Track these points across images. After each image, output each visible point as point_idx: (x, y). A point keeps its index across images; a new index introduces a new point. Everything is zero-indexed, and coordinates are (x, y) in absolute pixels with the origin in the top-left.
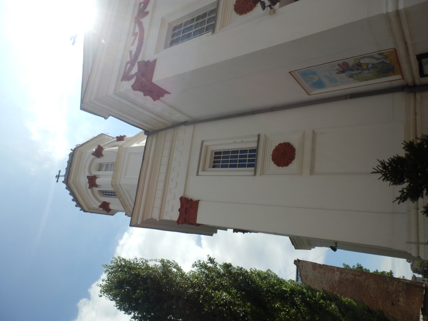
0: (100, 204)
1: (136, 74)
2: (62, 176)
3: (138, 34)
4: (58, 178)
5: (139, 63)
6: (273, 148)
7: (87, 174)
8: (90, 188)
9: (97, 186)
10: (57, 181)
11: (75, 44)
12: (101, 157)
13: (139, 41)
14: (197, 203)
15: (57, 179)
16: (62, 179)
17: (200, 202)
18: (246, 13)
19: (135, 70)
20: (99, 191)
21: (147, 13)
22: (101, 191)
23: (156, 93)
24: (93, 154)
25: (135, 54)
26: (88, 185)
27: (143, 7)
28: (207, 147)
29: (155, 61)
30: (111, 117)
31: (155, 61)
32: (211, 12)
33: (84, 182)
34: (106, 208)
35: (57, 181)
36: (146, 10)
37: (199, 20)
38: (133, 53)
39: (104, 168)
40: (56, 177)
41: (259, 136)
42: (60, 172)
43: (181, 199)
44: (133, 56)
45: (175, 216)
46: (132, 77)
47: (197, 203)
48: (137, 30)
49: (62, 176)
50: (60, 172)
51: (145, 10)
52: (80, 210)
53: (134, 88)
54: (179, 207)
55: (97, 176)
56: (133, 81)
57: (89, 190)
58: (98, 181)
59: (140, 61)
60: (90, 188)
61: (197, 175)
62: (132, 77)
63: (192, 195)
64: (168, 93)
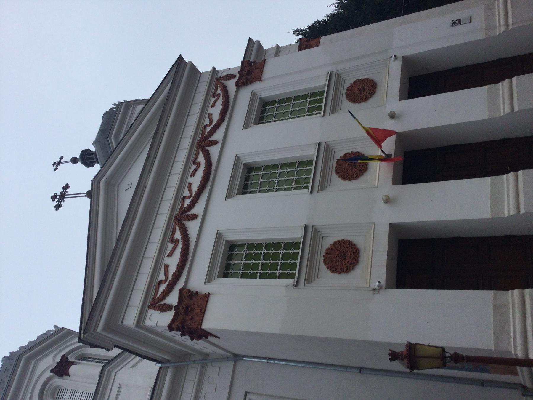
12: (65, 377)
18: (360, 102)
19: (173, 299)
31: (207, 297)
36: (193, 212)
46: (168, 308)
53: (171, 327)
56: (169, 316)
62: (168, 308)
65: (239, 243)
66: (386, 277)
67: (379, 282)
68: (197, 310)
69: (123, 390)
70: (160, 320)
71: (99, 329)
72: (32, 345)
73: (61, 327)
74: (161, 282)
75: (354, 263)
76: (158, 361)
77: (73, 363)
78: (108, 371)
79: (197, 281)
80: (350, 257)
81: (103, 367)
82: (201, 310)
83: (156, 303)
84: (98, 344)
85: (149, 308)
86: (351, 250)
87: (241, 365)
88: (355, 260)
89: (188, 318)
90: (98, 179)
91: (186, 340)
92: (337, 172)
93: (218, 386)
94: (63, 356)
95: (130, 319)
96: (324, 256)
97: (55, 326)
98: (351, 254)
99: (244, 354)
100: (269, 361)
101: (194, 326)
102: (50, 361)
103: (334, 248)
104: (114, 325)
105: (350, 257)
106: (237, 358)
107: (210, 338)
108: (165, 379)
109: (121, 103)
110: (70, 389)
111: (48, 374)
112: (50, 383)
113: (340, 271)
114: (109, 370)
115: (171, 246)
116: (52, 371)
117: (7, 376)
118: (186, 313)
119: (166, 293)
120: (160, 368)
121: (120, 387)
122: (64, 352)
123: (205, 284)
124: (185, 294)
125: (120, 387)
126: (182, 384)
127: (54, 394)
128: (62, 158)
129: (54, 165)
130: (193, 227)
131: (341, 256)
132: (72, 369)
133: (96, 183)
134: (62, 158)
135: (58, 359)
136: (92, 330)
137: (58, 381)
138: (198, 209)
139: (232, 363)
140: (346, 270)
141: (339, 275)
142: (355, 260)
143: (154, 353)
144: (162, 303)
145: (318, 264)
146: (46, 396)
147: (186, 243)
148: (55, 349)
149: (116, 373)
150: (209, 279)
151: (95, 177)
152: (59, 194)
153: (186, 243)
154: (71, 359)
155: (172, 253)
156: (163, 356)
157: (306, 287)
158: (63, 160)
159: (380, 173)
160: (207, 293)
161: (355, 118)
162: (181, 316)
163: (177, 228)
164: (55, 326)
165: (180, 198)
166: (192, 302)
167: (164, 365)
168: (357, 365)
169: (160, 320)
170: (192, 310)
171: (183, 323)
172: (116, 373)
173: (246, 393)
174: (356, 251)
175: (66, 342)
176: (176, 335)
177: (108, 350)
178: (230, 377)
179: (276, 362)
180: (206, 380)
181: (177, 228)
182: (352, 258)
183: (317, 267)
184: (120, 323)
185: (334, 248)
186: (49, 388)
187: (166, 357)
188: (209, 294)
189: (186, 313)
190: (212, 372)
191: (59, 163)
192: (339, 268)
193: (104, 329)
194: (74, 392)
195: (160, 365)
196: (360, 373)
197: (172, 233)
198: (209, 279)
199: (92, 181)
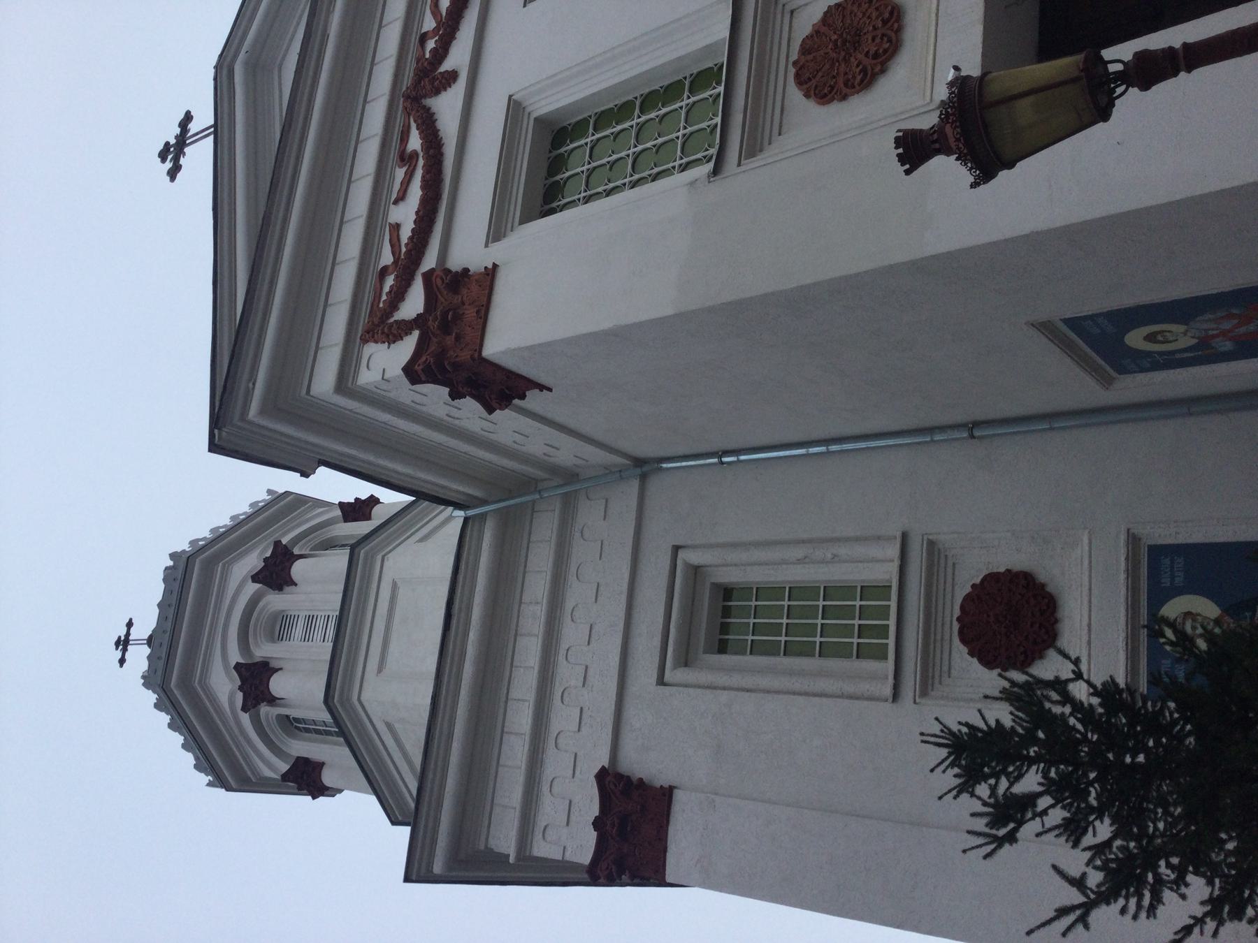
0: (284, 767)
1: (419, 322)
2: (138, 642)
3: (421, 162)
4: (125, 650)
5: (427, 277)
6: (963, 590)
7: (235, 657)
8: (245, 709)
9: (273, 701)
10: (122, 661)
11: (182, 116)
12: (287, 589)
13: (423, 188)
14: (666, 795)
15: (119, 654)
16: (139, 657)
17: (676, 791)
18: (844, 98)
19: (414, 304)
20: (279, 717)
21: (452, 76)
22: (287, 717)
23: (500, 387)
24: (255, 578)
25: (411, 239)
26: (239, 696)
27: (434, 51)
28: (696, 571)
29: (491, 273)
30: (322, 470)
31: (491, 273)
32: (702, 79)
33: (224, 686)
34: (306, 779)
35: (122, 661)
36: (447, 66)
37: (654, 107)
38: (406, 233)
39: (298, 631)
40: (117, 644)
41: (905, 537)
42: (130, 624)
43: (602, 776)
44: (404, 249)
45: (581, 844)
46: (404, 328)
47: (666, 795)
48: (415, 142)
49: (138, 642)
50: (130, 624)
51: (440, 62)
52: (210, 784)
53: (412, 373)
54: (596, 811)
55: (274, 664)
56: (407, 346)
57: (245, 718)
58: (277, 685)
59: (432, 270)
60: (245, 709)
61: (661, 681)
62: (404, 328)
63: (647, 762)
64: (542, 387)
65: (574, 120)
66: (984, 55)
67: (956, 68)
68: (470, 312)
69: (402, 592)
70: (386, 362)
71: (253, 413)
72: (219, 536)
73: (281, 491)
74: (384, 272)
75: (885, 51)
76: (458, 506)
78: (366, 558)
79: (468, 246)
80: (873, 40)
82: (478, 312)
83: (378, 325)
84: (276, 460)
85: (365, 341)
86: (874, 15)
87: (654, 484)
88: (890, 41)
89: (450, 340)
90: (229, 59)
91: (469, 411)
93: (606, 543)
95: (324, 381)
96: (795, 63)
97: (270, 492)
98: (875, 28)
99: (662, 454)
100: (725, 459)
101: (465, 355)
102: (253, 561)
103: (824, 29)
104: (287, 398)
105: (873, 40)
106: (644, 468)
107: (533, 400)
108: (479, 548)
110: (302, 614)
112: (261, 604)
113: (845, 90)
114: (367, 554)
115: (400, 173)
118: (446, 327)
119: (399, 295)
120: (466, 520)
121: (395, 587)
123: (486, 246)
124: (439, 282)
125: (395, 587)
126: (523, 552)
127: (272, 633)
130: (447, 106)
131: (844, 42)
132: (298, 569)
133: (225, 72)
136: (236, 420)
137: (275, 601)
138: (459, 57)
139: (635, 484)
140: (862, 81)
141: (844, 105)
142: (890, 41)
143: (430, 478)
144: (392, 320)
145: (780, 89)
146: (255, 634)
147: (432, 152)
150: (496, 232)
151: (221, 56)
152: (173, 141)
153: (432, 152)
155: (405, 191)
156: (461, 489)
157: (742, 168)
160: (490, 266)
162: (435, 340)
163: (413, 126)
164: (270, 492)
165: (414, 39)
166: (457, 299)
167: (470, 513)
168: (959, 417)
169: (386, 362)
170: (458, 317)
171: (441, 354)
173: (676, 549)
174: (891, 13)
176: (434, 397)
177: (305, 474)
178: (632, 516)
179: (742, 458)
180: (577, 535)
181: (413, 126)
182: (878, 40)
183: (779, 98)
184: (304, 391)
185: (824, 29)
186: (257, 620)
187: (470, 491)
188: (495, 266)
189: (446, 327)
190: (589, 515)
192: (841, 80)
193: (263, 411)
194: (311, 619)
195: (461, 513)
196: (972, 437)
197: (402, 140)
198: (496, 232)
199: (216, 67)
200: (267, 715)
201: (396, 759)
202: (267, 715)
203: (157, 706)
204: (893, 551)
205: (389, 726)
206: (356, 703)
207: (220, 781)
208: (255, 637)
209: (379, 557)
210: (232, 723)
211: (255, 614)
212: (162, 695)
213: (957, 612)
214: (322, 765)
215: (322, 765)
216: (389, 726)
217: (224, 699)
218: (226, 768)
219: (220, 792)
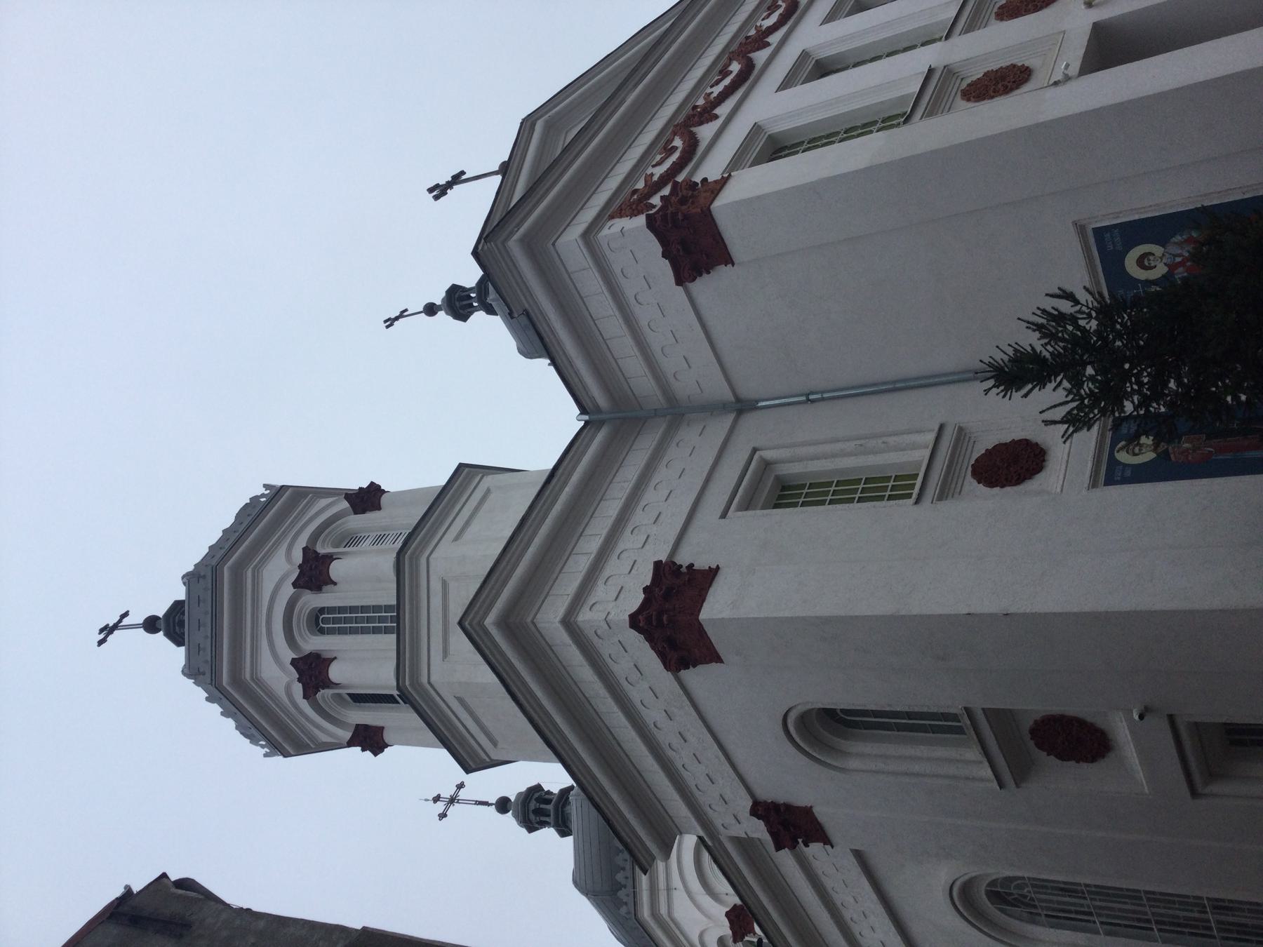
12: (325, 588)
18: (992, 97)
20: (334, 696)
28: (767, 465)
41: (942, 427)
58: (335, 673)
77: (330, 558)
81: (400, 553)
92: (1039, 746)
94: (305, 550)
97: (266, 486)
102: (280, 568)
109: (283, 488)
111: (291, 590)
114: (411, 558)
116: (295, 585)
117: (206, 613)
121: (445, 584)
122: (302, 542)
125: (445, 584)
128: (126, 615)
129: (101, 631)
134: (126, 615)
135: (298, 557)
148: (284, 534)
149: (428, 559)
154: (322, 549)
158: (126, 621)
159: (1136, 759)
161: (1055, 406)
164: (266, 486)
172: (428, 559)
175: (297, 518)
191: (116, 627)
200: (323, 697)
201: (454, 709)
202: (323, 697)
203: (222, 714)
204: (930, 437)
205: (461, 700)
206: (668, 919)
207: (276, 748)
208: (301, 636)
209: (423, 561)
210: (293, 710)
211: (296, 611)
212: (212, 688)
213: (973, 462)
214: (382, 729)
215: (382, 729)
216: (461, 700)
217: (280, 690)
218: (281, 736)
219: (279, 759)
